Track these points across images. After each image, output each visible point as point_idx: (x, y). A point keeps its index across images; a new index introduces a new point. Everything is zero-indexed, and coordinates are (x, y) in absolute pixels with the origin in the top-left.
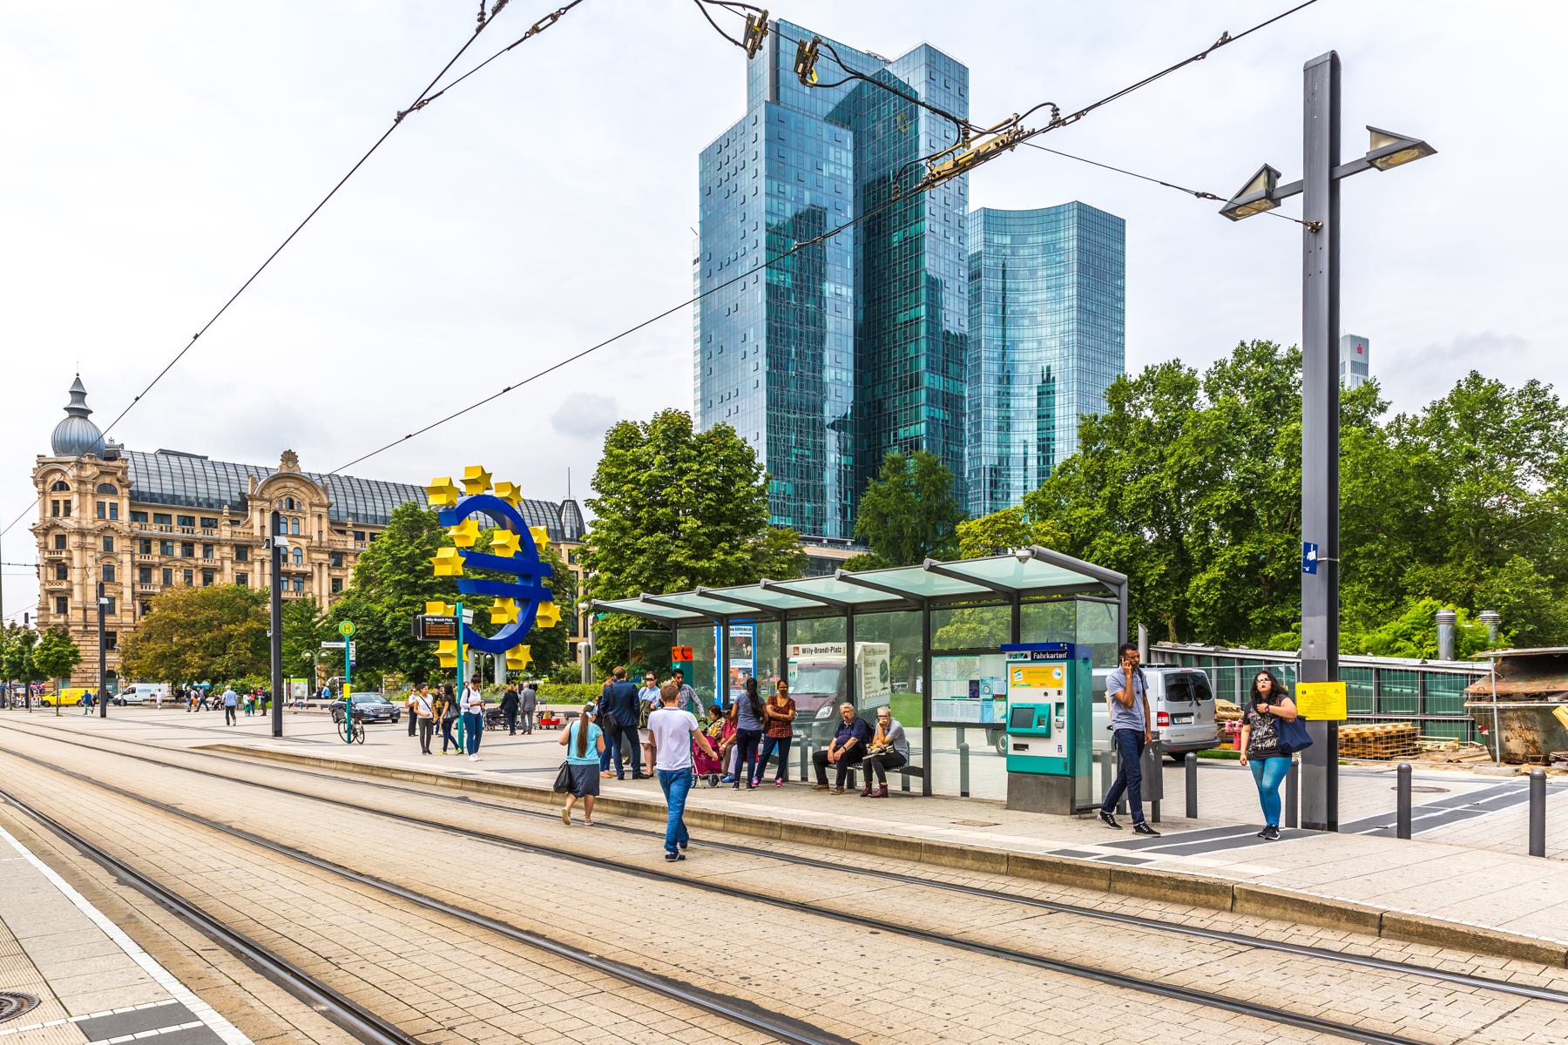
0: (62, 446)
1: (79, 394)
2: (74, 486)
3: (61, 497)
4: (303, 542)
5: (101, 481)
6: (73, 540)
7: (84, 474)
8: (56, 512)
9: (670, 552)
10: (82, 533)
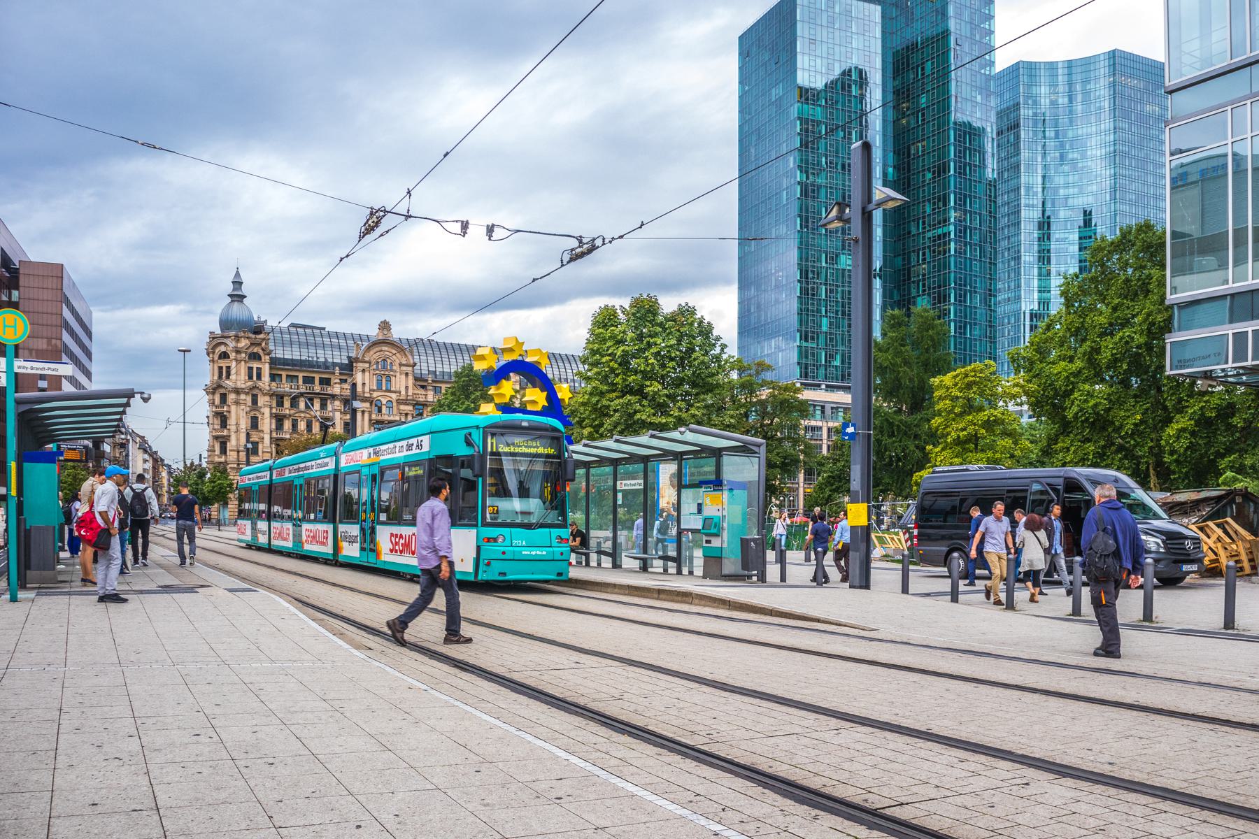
0: (226, 324)
1: (238, 284)
2: (233, 355)
3: (224, 363)
4: (394, 396)
5: (250, 350)
6: (231, 397)
7: (240, 345)
8: (220, 376)
9: (636, 412)
10: (237, 391)
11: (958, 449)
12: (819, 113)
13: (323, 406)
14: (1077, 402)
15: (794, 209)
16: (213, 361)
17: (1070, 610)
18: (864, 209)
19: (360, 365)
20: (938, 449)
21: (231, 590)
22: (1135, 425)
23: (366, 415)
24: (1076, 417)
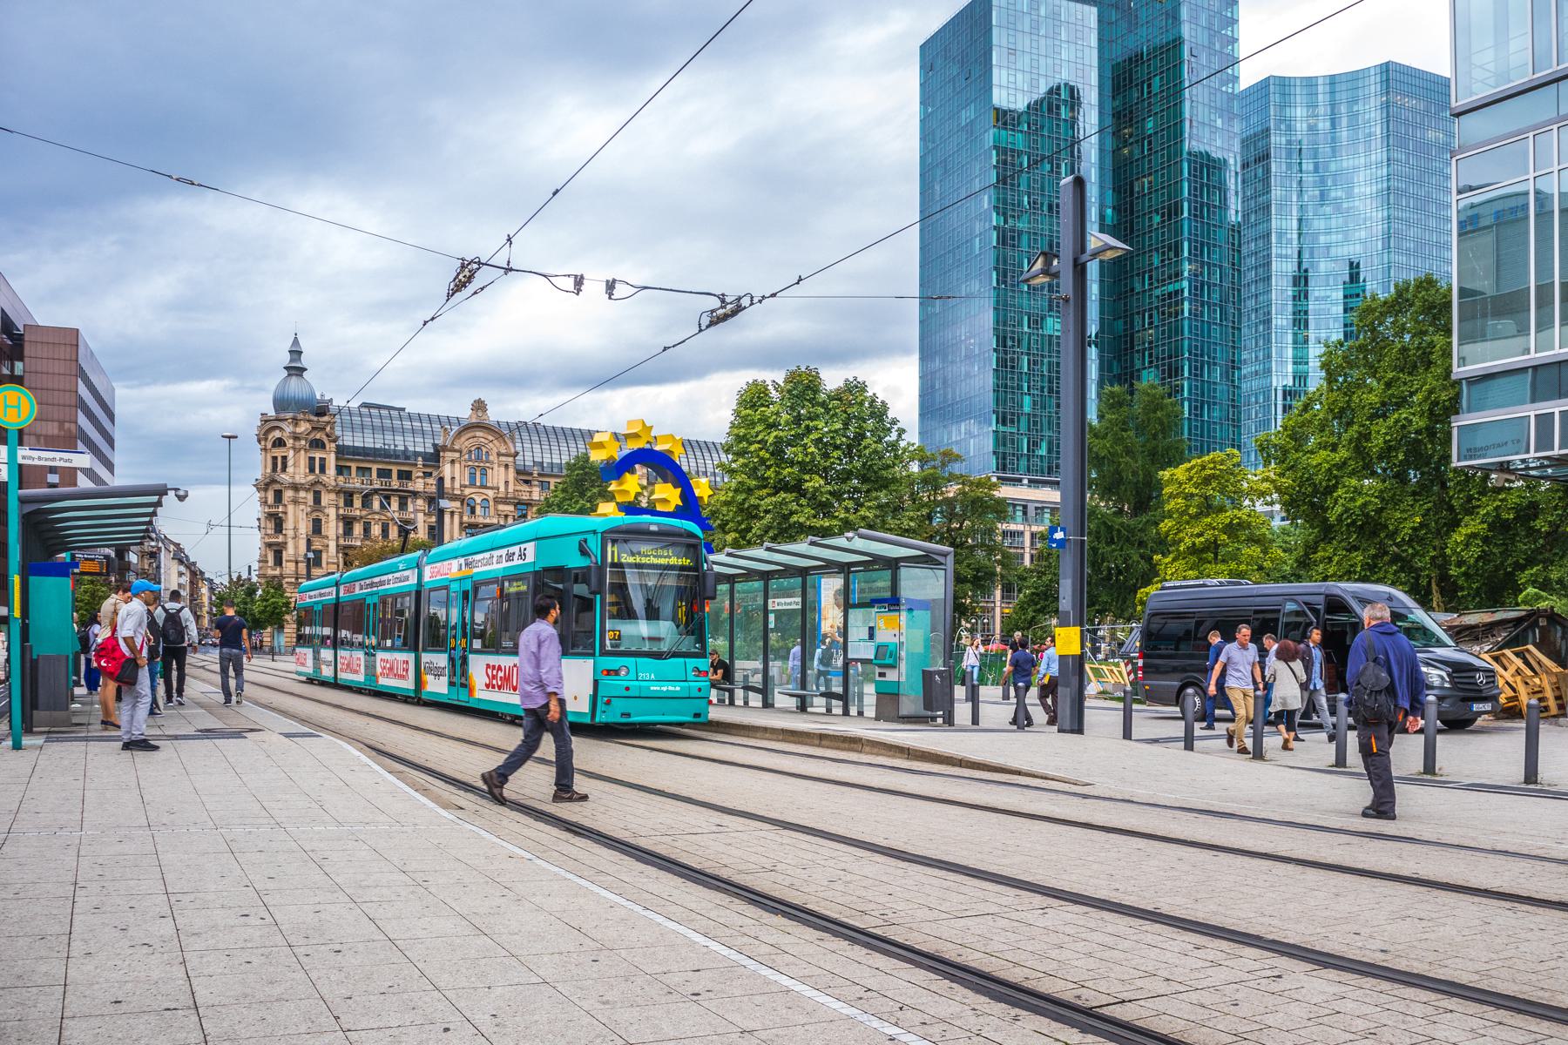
0: (281, 403)
1: (296, 353)
2: (290, 442)
3: (279, 452)
4: (491, 493)
5: (311, 437)
6: (288, 494)
7: (299, 430)
8: (274, 469)
9: (792, 513)
10: (296, 488)
11: (1194, 559)
12: (1019, 141)
13: (403, 506)
14: (1341, 501)
15: (989, 260)
16: (265, 449)
17: (1332, 760)
18: (1075, 260)
19: (448, 454)
20: (1168, 560)
21: (287, 735)
22: (1414, 529)
23: (456, 517)
24: (1340, 519)
